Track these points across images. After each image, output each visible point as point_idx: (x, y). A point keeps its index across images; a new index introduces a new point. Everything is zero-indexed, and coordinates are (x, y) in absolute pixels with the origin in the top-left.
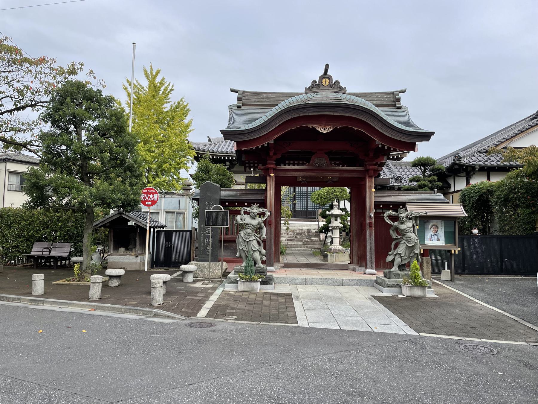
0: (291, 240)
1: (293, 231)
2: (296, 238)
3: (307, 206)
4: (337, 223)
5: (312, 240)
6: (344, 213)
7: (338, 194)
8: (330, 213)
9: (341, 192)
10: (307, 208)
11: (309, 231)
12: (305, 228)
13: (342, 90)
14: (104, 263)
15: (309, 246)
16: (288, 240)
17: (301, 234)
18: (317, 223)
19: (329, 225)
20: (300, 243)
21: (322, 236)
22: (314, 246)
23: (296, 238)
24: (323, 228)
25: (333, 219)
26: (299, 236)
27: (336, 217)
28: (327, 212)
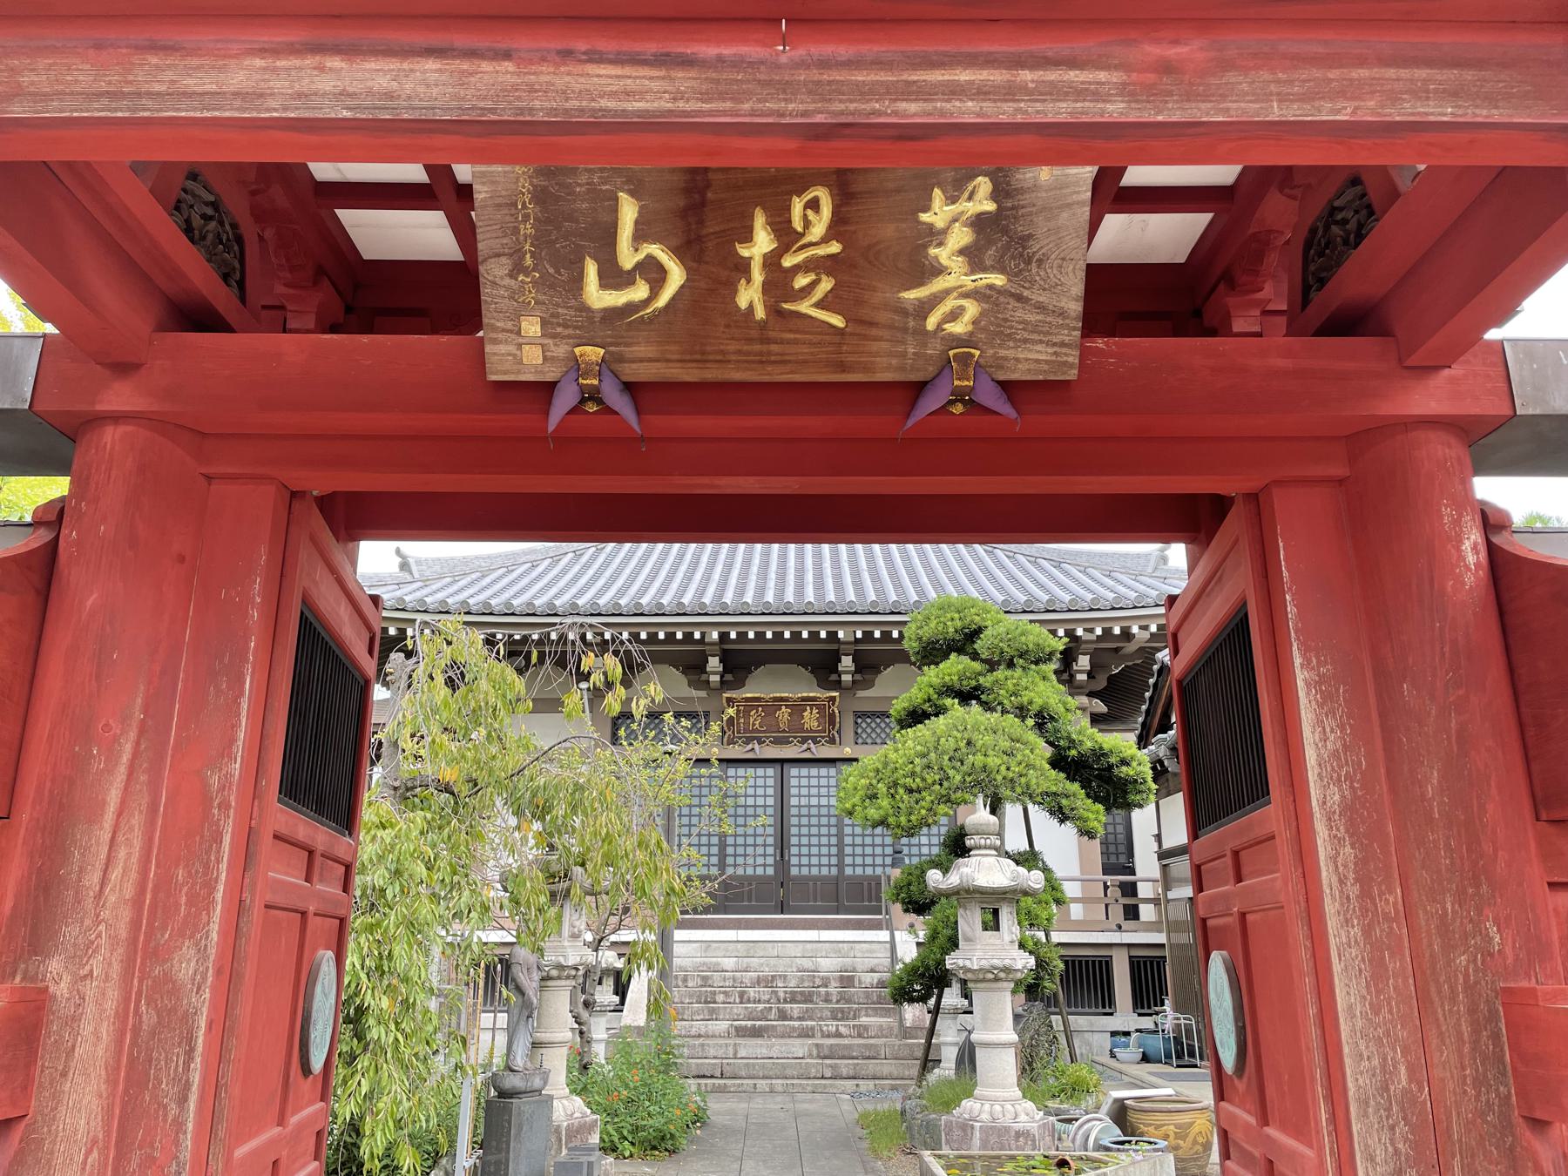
0: (756, 1033)
1: (768, 982)
2: (783, 1016)
3: (841, 855)
4: (994, 949)
5: (861, 1031)
6: (1035, 879)
7: (993, 761)
8: (953, 879)
9: (1009, 754)
10: (841, 866)
11: (847, 981)
12: (828, 964)
13: (373, 764)
14: (1065, 676)
15: (845, 1066)
16: (741, 1032)
17: (807, 998)
18: (884, 935)
19: (950, 962)
20: (799, 1047)
21: (913, 1013)
22: (872, 1066)
23: (783, 1016)
24: (913, 971)
25: (970, 921)
26: (795, 1009)
27: (992, 904)
28: (934, 877)
